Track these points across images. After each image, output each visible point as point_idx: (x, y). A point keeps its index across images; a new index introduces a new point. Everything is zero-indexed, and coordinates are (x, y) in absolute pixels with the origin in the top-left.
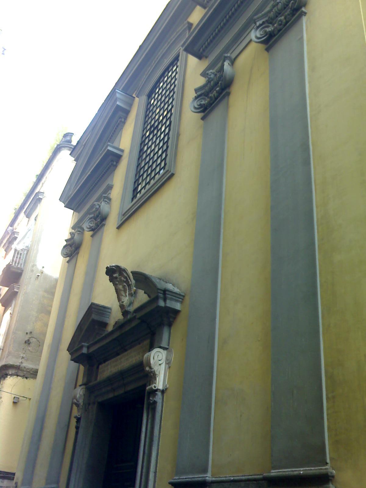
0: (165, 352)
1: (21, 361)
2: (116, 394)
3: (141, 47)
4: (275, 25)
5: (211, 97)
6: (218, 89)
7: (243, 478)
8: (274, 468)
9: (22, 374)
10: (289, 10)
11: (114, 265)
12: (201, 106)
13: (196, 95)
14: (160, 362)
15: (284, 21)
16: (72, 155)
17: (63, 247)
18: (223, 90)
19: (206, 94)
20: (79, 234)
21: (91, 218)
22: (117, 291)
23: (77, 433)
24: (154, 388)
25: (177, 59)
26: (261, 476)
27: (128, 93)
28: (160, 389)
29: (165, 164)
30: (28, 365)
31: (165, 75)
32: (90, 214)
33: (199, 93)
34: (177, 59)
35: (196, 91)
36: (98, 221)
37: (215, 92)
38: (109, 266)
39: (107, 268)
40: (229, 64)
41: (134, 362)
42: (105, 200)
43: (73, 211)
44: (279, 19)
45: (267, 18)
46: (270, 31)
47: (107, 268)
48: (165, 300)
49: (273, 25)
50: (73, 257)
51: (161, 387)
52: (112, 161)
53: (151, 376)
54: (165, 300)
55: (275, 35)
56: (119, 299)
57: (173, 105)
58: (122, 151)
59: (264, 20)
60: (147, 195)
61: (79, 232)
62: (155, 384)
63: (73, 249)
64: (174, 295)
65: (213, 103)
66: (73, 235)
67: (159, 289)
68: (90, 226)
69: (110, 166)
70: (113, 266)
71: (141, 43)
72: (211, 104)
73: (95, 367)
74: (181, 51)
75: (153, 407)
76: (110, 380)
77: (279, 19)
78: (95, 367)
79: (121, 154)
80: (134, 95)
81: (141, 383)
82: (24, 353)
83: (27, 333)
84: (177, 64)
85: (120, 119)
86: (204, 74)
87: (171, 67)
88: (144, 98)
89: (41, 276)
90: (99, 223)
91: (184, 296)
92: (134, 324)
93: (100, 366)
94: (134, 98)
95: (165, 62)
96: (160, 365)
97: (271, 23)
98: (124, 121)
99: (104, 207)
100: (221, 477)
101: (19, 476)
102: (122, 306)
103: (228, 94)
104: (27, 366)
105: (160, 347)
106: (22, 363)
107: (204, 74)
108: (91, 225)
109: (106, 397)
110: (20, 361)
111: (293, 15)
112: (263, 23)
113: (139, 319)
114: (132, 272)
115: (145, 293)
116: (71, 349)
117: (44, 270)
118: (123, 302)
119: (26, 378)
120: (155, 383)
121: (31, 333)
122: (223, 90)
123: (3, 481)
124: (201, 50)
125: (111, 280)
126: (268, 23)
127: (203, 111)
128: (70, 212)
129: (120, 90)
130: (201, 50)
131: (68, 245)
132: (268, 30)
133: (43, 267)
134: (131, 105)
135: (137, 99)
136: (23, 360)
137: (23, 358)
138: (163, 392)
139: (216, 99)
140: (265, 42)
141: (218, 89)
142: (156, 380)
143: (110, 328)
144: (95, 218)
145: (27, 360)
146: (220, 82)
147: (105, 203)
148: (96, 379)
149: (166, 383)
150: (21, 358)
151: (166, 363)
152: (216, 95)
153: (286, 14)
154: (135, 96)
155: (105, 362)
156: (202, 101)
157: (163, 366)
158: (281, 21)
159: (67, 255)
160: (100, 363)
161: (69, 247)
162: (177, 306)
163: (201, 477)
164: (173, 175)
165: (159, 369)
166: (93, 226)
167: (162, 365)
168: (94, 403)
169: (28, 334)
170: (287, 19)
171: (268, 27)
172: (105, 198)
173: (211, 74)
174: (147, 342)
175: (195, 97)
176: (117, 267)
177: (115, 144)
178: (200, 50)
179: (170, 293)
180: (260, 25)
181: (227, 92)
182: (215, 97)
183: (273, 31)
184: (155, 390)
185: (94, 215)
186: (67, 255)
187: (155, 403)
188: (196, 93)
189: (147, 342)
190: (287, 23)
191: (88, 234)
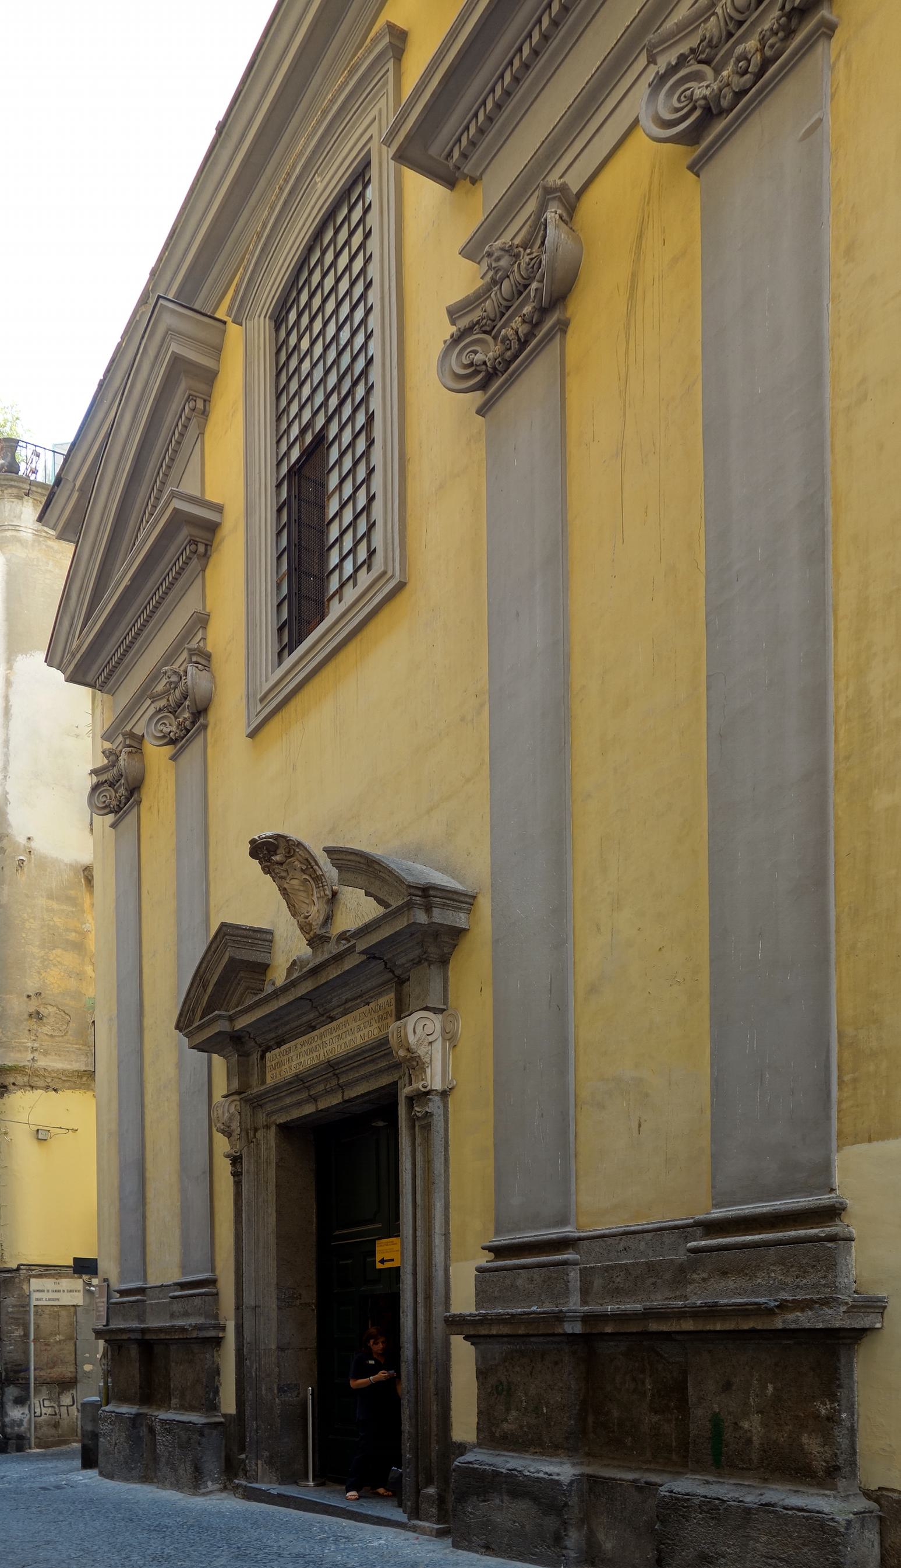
0: (440, 1016)
1: (32, 1057)
2: (322, 1105)
3: (222, 128)
4: (725, 73)
5: (506, 338)
6: (527, 309)
7: (651, 1226)
8: (715, 1206)
9: (41, 1083)
10: (776, 13)
11: (269, 833)
12: (474, 368)
13: (454, 329)
14: (431, 1039)
15: (757, 59)
16: (44, 520)
17: (89, 789)
18: (544, 311)
19: (488, 327)
20: (130, 752)
21: (160, 710)
22: (284, 892)
23: (238, 1184)
24: (423, 1089)
25: (361, 176)
26: (691, 1221)
27: (196, 307)
28: (436, 1090)
29: (371, 553)
30: (51, 1064)
31: (326, 242)
32: (154, 698)
33: (464, 323)
34: (361, 176)
35: (454, 313)
36: (185, 718)
37: (518, 319)
38: (256, 837)
39: (253, 842)
40: (561, 217)
41: (359, 1041)
42: (194, 659)
43: (90, 690)
44: (740, 49)
45: (693, 42)
46: (705, 98)
47: (253, 842)
48: (428, 909)
49: (717, 71)
50: (126, 813)
51: (437, 1085)
52: (193, 542)
53: (414, 1064)
54: (428, 909)
55: (723, 112)
56: (294, 912)
57: (370, 355)
58: (219, 509)
59: (683, 48)
60: (117, 468)
61: (129, 749)
62: (423, 1082)
63: (122, 791)
64: (450, 895)
65: (516, 357)
66: (112, 758)
67: (410, 887)
68: (161, 731)
69: (189, 558)
70: (270, 837)
71: (220, 117)
72: (509, 363)
73: (255, 1057)
74: (374, 145)
75: (423, 1125)
76: (301, 1081)
77: (740, 49)
78: (255, 1057)
79: (218, 520)
80: (221, 314)
81: (384, 1081)
82: (35, 1040)
83: (29, 996)
84: (362, 196)
85: (192, 404)
86: (470, 251)
87: (345, 211)
88: (261, 326)
89: (29, 861)
90: (187, 723)
91: (474, 897)
92: (348, 964)
93: (268, 1055)
94: (225, 323)
95: (320, 187)
96: (430, 1043)
97: (707, 62)
98: (205, 406)
99: (196, 679)
100: (599, 1230)
101: (109, 1267)
102: (305, 927)
103: (563, 326)
104: (50, 1066)
105: (427, 1009)
106: (37, 1061)
107: (470, 251)
108: (166, 730)
109: (296, 1114)
110: (30, 1056)
111: (789, 33)
112: (682, 60)
113: (362, 952)
114: (329, 851)
115: (367, 894)
116: (183, 1024)
117: (33, 844)
118: (307, 917)
119: (55, 1090)
120: (423, 1080)
121: (38, 994)
122: (544, 311)
123: (58, 1281)
124: (456, 154)
125: (267, 870)
126: (700, 62)
127: (483, 386)
128: (82, 694)
129: (170, 297)
130: (456, 154)
131: (103, 783)
132: (700, 90)
133: (29, 839)
134: (217, 350)
135: (233, 329)
136: (36, 1054)
137: (34, 1050)
138: (444, 1094)
139: (523, 344)
140: (691, 137)
141: (527, 309)
142: (425, 1072)
143: (279, 976)
144: (174, 710)
145: (46, 1053)
146: (534, 285)
147: (197, 667)
148: (263, 1082)
149: (450, 1078)
150: (30, 1051)
151: (444, 1040)
152: (523, 330)
153: (767, 26)
154: (225, 318)
155: (279, 1045)
156: (475, 352)
157: (438, 1046)
158: (745, 57)
159: (108, 810)
160: (269, 1049)
161: (106, 787)
162: (460, 920)
163: (554, 1233)
164: (401, 586)
165: (430, 1053)
166: (170, 732)
167: (434, 1045)
168: (267, 1127)
169: (32, 998)
170: (768, 52)
171: (697, 76)
172: (194, 654)
173: (502, 253)
174: (388, 999)
175: (452, 336)
176: (278, 837)
177: (189, 487)
178: (450, 155)
179: (438, 894)
180: (673, 69)
181: (559, 322)
182: (519, 339)
183: (718, 96)
184: (424, 1092)
185: (168, 700)
186: (108, 810)
187: (428, 1115)
188: (453, 323)
189: (388, 999)
190: (766, 64)
191: (157, 754)
